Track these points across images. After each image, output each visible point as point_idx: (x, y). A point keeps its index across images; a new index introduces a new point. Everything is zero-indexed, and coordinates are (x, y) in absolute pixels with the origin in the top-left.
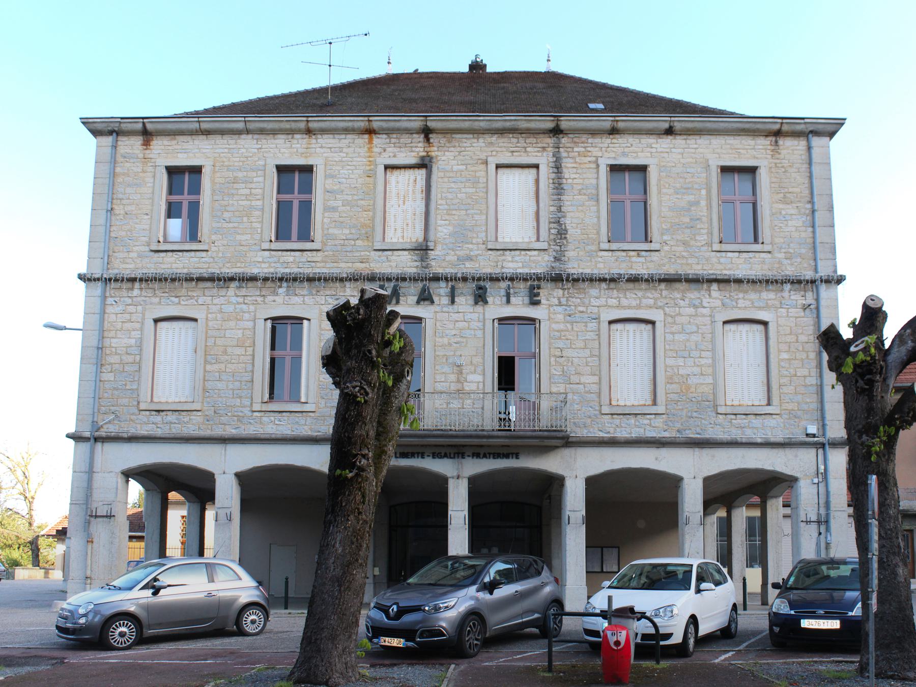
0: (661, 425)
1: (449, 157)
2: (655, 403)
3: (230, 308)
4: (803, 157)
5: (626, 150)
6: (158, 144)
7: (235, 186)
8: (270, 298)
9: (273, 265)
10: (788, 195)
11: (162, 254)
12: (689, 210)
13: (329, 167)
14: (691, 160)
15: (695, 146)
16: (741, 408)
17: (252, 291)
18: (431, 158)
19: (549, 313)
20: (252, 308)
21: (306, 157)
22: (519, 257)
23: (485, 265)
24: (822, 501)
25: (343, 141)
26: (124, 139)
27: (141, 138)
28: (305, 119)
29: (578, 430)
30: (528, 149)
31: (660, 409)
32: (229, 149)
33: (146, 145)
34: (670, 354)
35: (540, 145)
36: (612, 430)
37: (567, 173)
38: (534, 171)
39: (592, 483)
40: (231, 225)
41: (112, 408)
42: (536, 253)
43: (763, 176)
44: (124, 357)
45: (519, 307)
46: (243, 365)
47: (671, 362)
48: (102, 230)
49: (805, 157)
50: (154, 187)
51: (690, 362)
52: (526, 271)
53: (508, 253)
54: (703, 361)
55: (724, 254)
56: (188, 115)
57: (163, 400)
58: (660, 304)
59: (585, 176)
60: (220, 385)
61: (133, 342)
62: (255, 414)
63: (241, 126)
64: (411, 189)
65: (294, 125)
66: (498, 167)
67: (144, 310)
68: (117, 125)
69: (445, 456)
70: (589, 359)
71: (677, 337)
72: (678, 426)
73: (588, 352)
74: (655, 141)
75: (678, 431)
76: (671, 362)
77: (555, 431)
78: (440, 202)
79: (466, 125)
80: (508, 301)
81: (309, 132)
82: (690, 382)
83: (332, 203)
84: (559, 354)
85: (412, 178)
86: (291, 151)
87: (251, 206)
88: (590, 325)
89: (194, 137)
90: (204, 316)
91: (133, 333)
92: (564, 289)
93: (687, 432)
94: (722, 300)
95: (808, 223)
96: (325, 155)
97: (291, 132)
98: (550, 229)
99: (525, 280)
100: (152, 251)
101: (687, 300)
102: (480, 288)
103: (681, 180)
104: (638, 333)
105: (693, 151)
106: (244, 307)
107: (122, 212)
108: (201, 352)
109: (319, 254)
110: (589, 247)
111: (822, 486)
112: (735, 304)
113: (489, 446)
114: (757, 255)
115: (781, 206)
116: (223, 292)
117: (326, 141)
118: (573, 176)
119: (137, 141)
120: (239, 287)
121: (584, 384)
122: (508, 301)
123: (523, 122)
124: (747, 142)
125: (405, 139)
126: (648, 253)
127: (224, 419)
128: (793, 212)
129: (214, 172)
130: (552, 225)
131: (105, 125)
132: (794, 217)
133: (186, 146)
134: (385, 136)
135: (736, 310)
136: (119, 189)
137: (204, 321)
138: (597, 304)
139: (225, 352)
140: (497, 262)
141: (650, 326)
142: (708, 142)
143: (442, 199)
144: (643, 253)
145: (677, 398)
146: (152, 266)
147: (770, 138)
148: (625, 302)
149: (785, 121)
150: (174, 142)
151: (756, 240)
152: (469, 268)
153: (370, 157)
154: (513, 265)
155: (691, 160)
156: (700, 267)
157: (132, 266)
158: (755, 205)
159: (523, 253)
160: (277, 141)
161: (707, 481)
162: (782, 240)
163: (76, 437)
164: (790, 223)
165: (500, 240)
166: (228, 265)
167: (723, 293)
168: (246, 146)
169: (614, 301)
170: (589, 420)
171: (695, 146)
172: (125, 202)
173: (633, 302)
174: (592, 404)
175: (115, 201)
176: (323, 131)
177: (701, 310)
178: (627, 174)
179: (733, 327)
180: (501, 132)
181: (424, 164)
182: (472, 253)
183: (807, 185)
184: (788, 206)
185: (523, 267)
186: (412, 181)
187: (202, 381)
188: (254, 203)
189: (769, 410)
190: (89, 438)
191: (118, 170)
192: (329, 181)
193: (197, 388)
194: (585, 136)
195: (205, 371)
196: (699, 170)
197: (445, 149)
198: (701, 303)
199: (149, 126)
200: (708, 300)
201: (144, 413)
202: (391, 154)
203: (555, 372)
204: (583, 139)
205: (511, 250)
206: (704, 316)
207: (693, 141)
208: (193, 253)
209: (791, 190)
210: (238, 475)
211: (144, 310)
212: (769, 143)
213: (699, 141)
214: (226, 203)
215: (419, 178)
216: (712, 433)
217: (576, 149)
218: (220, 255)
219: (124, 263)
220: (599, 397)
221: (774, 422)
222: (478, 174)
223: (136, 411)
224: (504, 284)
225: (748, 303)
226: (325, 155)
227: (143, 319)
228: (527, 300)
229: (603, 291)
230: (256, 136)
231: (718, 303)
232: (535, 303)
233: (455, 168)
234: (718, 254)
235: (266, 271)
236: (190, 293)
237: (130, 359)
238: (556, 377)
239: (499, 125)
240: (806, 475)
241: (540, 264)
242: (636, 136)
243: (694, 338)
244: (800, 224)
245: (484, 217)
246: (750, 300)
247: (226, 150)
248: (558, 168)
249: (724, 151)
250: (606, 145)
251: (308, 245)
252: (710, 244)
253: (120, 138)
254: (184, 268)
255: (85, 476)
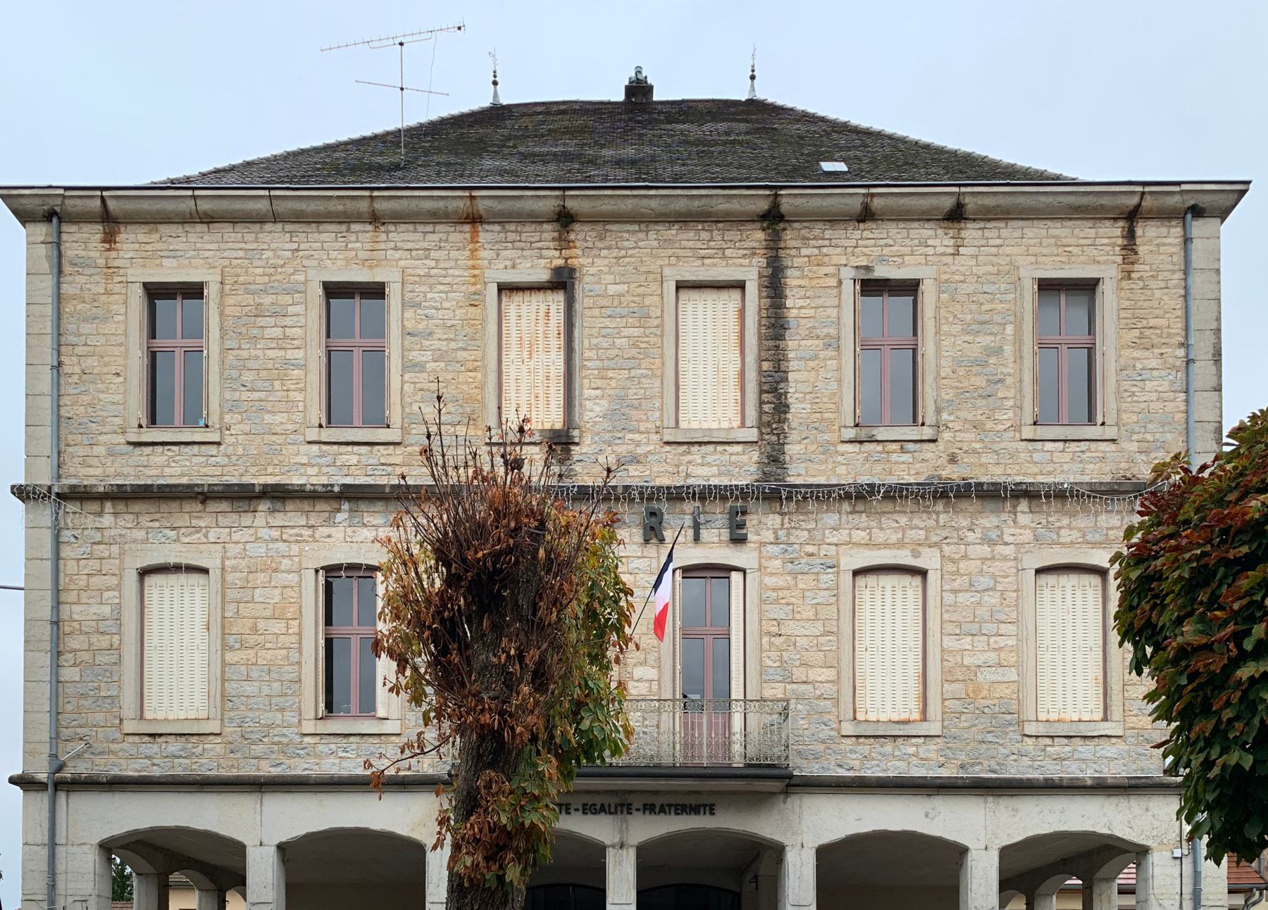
0: (933, 755)
1: (604, 266)
2: (924, 718)
3: (258, 550)
4: (1175, 259)
5: (886, 251)
6: (130, 238)
7: (261, 321)
8: (324, 531)
9: (325, 470)
10: (1148, 332)
11: (148, 450)
12: (984, 364)
13: (410, 287)
14: (989, 268)
15: (998, 242)
16: (1061, 726)
17: (293, 517)
18: (572, 271)
19: (760, 558)
20: (295, 548)
21: (371, 267)
22: (715, 456)
23: (660, 472)
24: (1188, 889)
25: (430, 237)
26: (74, 228)
27: (100, 227)
28: (367, 193)
29: (803, 763)
30: (728, 252)
31: (934, 728)
32: (246, 250)
33: (109, 242)
34: (949, 628)
35: (746, 245)
36: (856, 764)
37: (793, 301)
38: (736, 294)
39: (826, 855)
40: (256, 395)
41: (78, 730)
42: (738, 448)
43: (1108, 297)
44: (94, 639)
45: (714, 550)
46: (284, 652)
47: (949, 642)
48: (47, 402)
49: (1178, 259)
50: (126, 322)
51: (981, 642)
52: (725, 481)
53: (695, 448)
54: (1002, 642)
55: (1038, 445)
56: (172, 185)
57: (160, 716)
58: (934, 539)
59: (819, 302)
60: (249, 688)
61: (106, 610)
62: (307, 739)
63: (263, 206)
64: (541, 329)
65: (350, 206)
66: (681, 286)
67: (122, 553)
68: (59, 201)
69: (603, 810)
70: (823, 640)
71: (962, 597)
72: (963, 757)
73: (819, 624)
74: (931, 232)
75: (962, 767)
76: (949, 642)
77: (769, 766)
78: (587, 354)
79: (627, 206)
80: (697, 538)
81: (375, 219)
82: (980, 678)
83: (415, 355)
84: (775, 629)
85: (543, 308)
86: (344, 255)
87: (287, 363)
88: (823, 577)
89: (187, 227)
90: (218, 563)
91: (107, 595)
92: (782, 514)
93: (977, 768)
94: (1034, 530)
95: (1179, 385)
96: (402, 263)
97: (346, 219)
98: (761, 403)
99: (724, 498)
100: (129, 443)
101: (978, 530)
102: (653, 514)
103: (974, 307)
104: (899, 593)
105: (994, 250)
106: (282, 546)
107: (77, 370)
108: (216, 630)
109: (399, 450)
110: (826, 437)
111: (1187, 862)
112: (1055, 537)
113: (668, 792)
114: (1093, 445)
115: (1137, 354)
116: (247, 519)
117: (402, 236)
118: (801, 303)
119: (94, 233)
120: (273, 511)
121: (812, 683)
122: (697, 538)
123: (722, 203)
124: (1084, 231)
125: (529, 232)
126: (918, 446)
127: (258, 749)
128: (1153, 363)
129: (222, 294)
130: (765, 397)
131: (38, 201)
132: (1156, 373)
133: (176, 244)
134: (497, 228)
135: (1057, 549)
136: (69, 325)
137: (218, 572)
138: (834, 540)
139: (254, 630)
140: (677, 466)
141: (917, 580)
142: (1018, 233)
143: (590, 349)
144: (910, 446)
145: (961, 709)
146: (131, 471)
147: (1121, 223)
148: (879, 536)
149: (1147, 189)
150: (155, 237)
151: (1091, 419)
152: (633, 476)
153: (474, 267)
154: (705, 470)
155: (989, 268)
156: (999, 470)
157: (98, 472)
158: (1091, 351)
159: (720, 448)
160: (323, 237)
161: (1005, 852)
162: (1135, 418)
163: (24, 782)
164: (1149, 385)
165: (683, 425)
166: (253, 470)
167: (1037, 518)
168: (273, 246)
169: (863, 534)
170: (821, 747)
171: (998, 242)
172: (79, 350)
173: (891, 535)
174: (826, 717)
175: (63, 349)
176: (400, 218)
177: (1000, 549)
178: (738, 762)
179: (1051, 579)
180: (684, 219)
181: (562, 281)
182: (639, 450)
183: (1179, 313)
184: (1147, 353)
185: (720, 474)
186: (542, 314)
187: (219, 682)
188: (291, 354)
189: (1106, 729)
190: (51, 784)
191: (65, 288)
192: (409, 314)
193: (212, 693)
194: (820, 225)
195: (224, 664)
196: (1003, 287)
197: (595, 252)
198: (1001, 537)
199: (112, 205)
200: (1012, 531)
201: (131, 739)
202: (509, 263)
203: (769, 663)
204: (817, 232)
205: (700, 443)
206: (1005, 558)
207: (994, 233)
208: (196, 448)
209: (1153, 322)
210: (281, 848)
211: (122, 553)
212: (1118, 232)
213: (1004, 233)
214: (245, 354)
215: (553, 308)
216: (1013, 771)
217: (805, 252)
218: (240, 451)
219: (83, 464)
220: (837, 705)
221: (1114, 749)
222: (647, 302)
223: (118, 735)
224: (689, 506)
225: (1076, 535)
226: (402, 263)
227: (122, 569)
228: (725, 534)
229: (844, 517)
230: (289, 227)
231: (1027, 536)
232: (738, 540)
233: (612, 289)
234: (1030, 446)
235: (314, 481)
236: (194, 522)
237: (104, 642)
238: (771, 671)
239: (680, 205)
240: (1161, 843)
241: (742, 468)
242: (901, 225)
243: (992, 599)
244: (1165, 386)
245: (657, 383)
246: (1079, 530)
247: (241, 254)
248: (774, 286)
249: (1045, 251)
250: (853, 243)
251: (382, 435)
252: (1017, 428)
253: (65, 228)
254: (183, 475)
255: (44, 852)
